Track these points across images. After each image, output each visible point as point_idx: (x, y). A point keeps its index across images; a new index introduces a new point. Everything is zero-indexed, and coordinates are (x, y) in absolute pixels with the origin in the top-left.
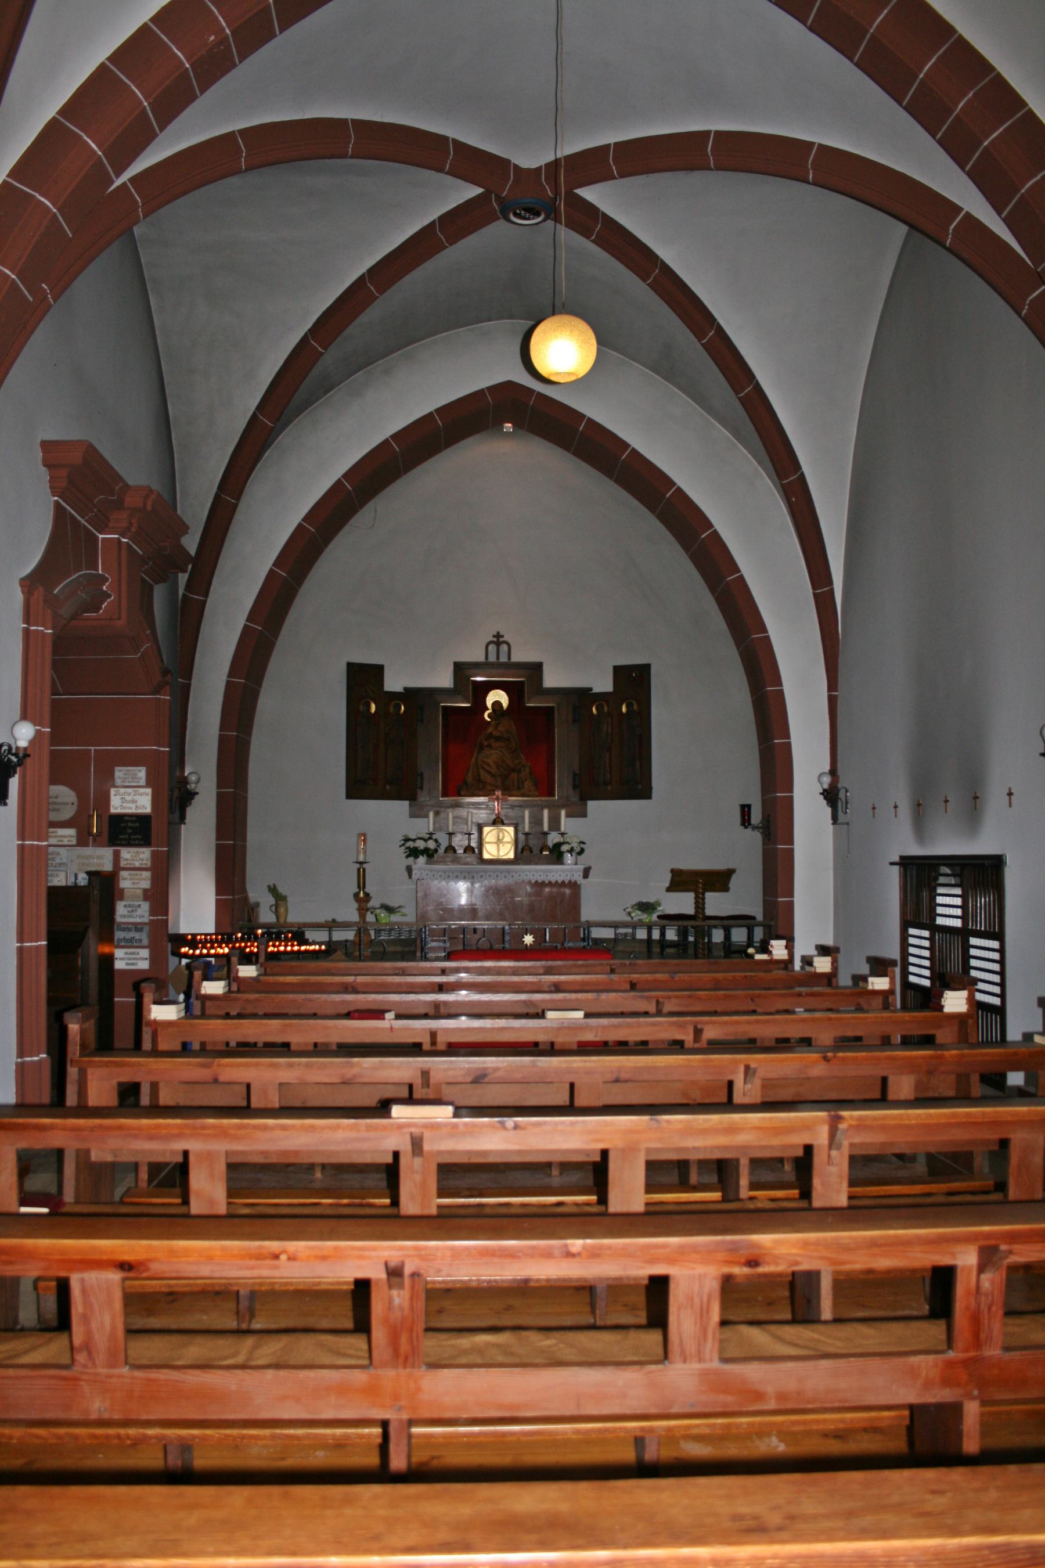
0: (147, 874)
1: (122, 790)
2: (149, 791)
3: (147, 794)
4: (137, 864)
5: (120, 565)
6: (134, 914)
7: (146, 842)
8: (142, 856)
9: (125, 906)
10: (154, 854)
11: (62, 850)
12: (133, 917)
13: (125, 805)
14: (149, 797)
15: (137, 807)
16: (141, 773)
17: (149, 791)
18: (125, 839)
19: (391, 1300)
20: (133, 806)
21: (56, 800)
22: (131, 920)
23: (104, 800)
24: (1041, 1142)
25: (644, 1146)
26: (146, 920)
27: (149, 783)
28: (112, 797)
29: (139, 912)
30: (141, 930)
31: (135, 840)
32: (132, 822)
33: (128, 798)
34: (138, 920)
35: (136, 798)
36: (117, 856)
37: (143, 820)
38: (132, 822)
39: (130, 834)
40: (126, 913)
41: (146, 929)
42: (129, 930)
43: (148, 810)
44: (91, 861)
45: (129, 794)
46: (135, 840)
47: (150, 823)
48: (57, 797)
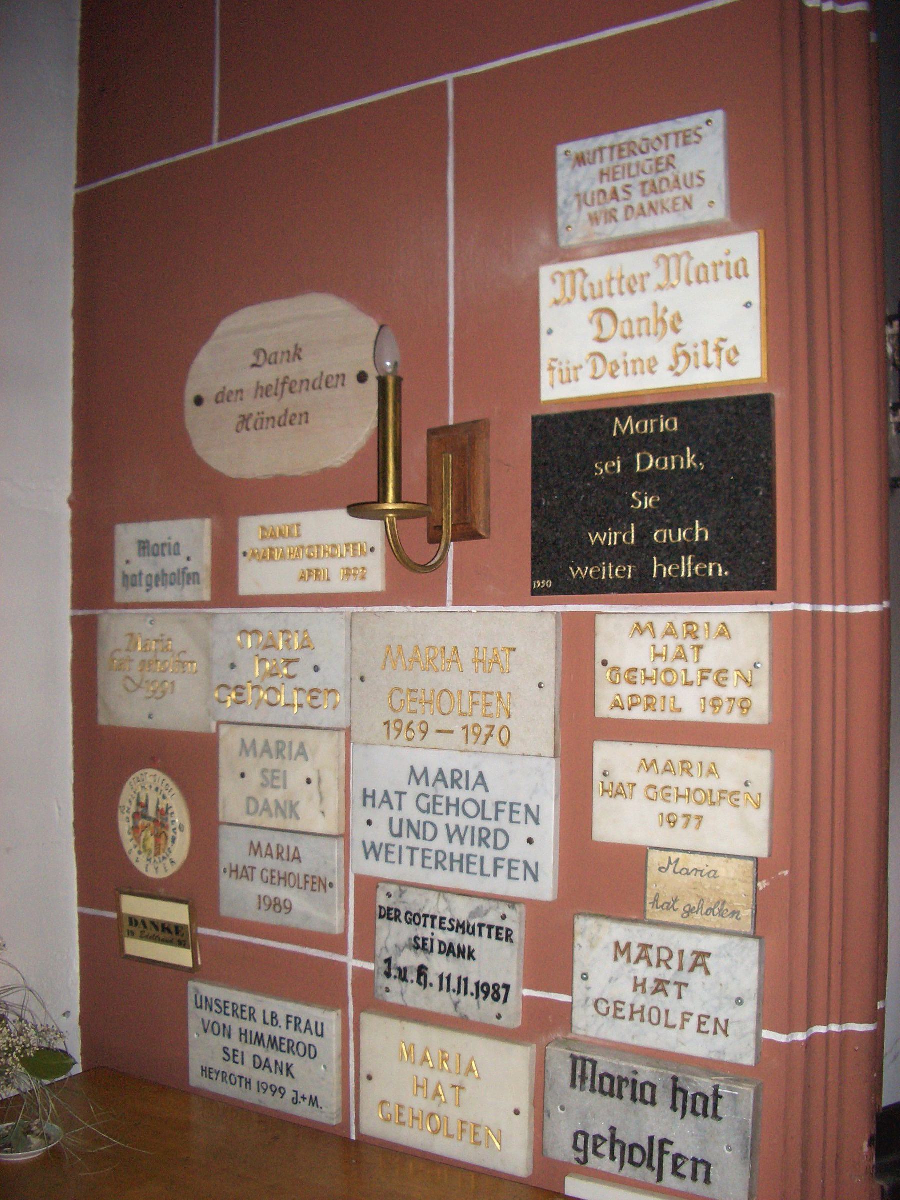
0: (754, 768)
1: (598, 268)
2: (747, 246)
3: (738, 272)
4: (690, 707)
5: (831, 382)
6: (668, 1001)
7: (747, 567)
8: (714, 655)
9: (621, 950)
10: (795, 649)
11: (328, 626)
12: (662, 1019)
13: (612, 350)
14: (751, 288)
15: (682, 354)
16: (701, 150)
17: (747, 246)
18: (618, 554)
19: (735, 535)
20: (662, 349)
21: (293, 370)
22: (653, 1037)
23: (513, 332)
24: (711, 821)
25: (449, 608)
26: (739, 1048)
27: (743, 211)
28: (548, 316)
29: (701, 994)
30: (706, 1106)
31: (672, 553)
32: (663, 444)
33: (628, 307)
34: (693, 1044)
35: (678, 299)
36: (578, 644)
37: (724, 436)
38: (663, 444)
39: (648, 521)
40: (625, 992)
41: (739, 1102)
42: (642, 1094)
43: (744, 365)
44: (450, 680)
45: (634, 285)
46: (672, 553)
47: (765, 442)
48: (297, 354)
